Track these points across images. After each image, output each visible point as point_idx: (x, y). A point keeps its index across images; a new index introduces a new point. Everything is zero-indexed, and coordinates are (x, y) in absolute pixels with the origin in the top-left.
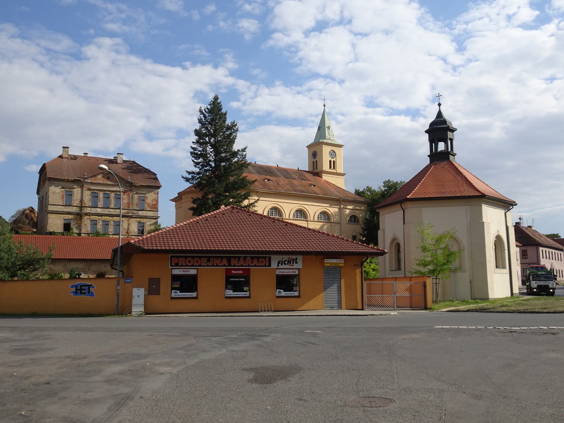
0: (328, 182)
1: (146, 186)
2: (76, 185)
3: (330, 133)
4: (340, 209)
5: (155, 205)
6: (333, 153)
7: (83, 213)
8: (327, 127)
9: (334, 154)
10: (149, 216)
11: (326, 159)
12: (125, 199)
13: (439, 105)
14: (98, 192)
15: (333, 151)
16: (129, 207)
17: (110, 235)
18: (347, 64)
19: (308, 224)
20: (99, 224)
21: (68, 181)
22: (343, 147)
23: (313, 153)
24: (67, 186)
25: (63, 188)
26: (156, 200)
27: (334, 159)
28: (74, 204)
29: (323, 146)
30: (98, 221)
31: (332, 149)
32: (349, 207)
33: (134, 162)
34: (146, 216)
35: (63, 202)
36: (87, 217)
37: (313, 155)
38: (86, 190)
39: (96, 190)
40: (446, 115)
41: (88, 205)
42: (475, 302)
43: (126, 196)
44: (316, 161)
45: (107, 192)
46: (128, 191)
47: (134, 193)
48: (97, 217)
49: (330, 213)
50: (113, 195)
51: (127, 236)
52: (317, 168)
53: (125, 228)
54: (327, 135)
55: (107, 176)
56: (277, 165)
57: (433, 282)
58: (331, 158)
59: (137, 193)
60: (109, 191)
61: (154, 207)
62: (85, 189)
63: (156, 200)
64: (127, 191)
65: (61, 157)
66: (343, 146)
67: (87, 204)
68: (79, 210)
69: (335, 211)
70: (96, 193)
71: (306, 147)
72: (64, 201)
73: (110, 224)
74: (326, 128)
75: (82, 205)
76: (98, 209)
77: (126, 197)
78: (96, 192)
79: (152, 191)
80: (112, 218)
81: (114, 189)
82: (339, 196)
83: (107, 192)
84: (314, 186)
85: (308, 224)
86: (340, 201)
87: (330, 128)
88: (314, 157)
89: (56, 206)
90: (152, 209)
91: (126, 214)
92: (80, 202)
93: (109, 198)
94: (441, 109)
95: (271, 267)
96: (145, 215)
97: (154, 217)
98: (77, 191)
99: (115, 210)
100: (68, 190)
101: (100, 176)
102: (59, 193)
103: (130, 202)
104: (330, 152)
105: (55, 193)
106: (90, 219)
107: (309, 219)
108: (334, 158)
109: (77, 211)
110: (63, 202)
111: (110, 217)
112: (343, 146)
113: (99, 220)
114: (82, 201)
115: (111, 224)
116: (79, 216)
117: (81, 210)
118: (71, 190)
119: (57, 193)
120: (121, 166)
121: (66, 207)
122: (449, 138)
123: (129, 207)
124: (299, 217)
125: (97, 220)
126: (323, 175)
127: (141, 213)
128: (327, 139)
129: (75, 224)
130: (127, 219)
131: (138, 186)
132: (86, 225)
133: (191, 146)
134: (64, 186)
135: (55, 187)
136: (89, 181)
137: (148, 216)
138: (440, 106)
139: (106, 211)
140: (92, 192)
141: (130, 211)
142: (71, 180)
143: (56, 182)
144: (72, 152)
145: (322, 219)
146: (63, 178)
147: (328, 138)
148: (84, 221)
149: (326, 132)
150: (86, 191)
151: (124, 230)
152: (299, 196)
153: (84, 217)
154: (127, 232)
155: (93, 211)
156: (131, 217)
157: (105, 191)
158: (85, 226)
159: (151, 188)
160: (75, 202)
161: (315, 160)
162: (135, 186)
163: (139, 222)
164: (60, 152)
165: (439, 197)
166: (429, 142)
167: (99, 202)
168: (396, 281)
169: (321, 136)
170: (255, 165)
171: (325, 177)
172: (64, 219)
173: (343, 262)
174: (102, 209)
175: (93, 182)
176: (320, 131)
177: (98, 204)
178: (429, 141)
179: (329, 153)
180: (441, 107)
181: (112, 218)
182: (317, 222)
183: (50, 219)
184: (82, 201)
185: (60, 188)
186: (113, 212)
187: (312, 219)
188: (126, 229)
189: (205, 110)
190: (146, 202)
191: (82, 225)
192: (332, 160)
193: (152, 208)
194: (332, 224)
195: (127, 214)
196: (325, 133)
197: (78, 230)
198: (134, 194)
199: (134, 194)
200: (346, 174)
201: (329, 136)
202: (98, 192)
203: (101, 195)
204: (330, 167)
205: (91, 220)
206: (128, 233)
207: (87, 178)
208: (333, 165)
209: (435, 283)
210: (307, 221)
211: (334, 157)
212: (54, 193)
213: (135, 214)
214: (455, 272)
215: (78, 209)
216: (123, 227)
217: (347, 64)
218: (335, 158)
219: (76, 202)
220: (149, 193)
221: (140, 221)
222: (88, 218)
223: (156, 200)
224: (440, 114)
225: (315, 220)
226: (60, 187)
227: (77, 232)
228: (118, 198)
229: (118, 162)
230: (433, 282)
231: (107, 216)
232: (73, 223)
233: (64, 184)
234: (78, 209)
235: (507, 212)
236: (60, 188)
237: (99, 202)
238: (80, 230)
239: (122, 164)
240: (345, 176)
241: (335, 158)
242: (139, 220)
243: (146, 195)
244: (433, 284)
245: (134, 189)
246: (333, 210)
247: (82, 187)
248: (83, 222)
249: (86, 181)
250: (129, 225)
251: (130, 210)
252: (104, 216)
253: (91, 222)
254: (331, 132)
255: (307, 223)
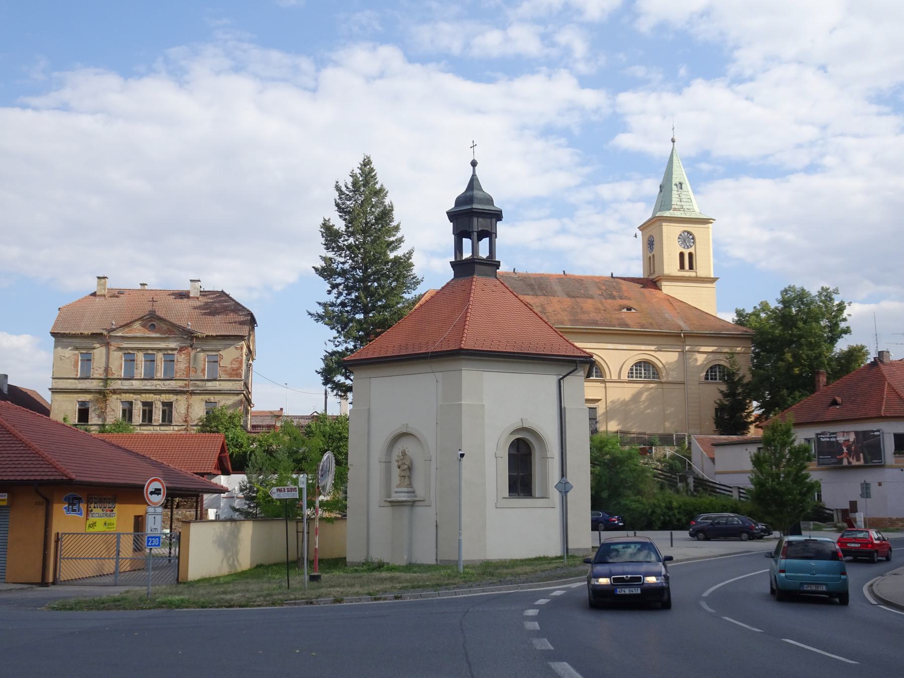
0: (671, 300)
1: (217, 336)
2: (98, 343)
3: (683, 196)
4: (683, 353)
5: (237, 370)
6: (687, 239)
7: (109, 389)
8: (676, 185)
9: (691, 237)
10: (224, 391)
11: (671, 250)
12: (181, 362)
14: (134, 352)
15: (688, 233)
16: (188, 375)
17: (155, 427)
18: (832, 30)
19: (605, 387)
20: (137, 408)
21: (82, 336)
22: (711, 223)
23: (649, 241)
24: (83, 345)
25: (76, 348)
26: (239, 360)
27: (692, 250)
28: (95, 376)
29: (663, 224)
30: (134, 403)
31: (686, 229)
32: (703, 349)
33: (222, 292)
34: (219, 390)
35: (75, 373)
36: (115, 396)
38: (115, 351)
39: (131, 349)
40: (487, 186)
41: (118, 376)
42: (513, 567)
43: (183, 356)
44: (653, 255)
45: (150, 352)
46: (186, 348)
47: (198, 350)
48: (132, 395)
49: (660, 365)
50: (160, 356)
51: (184, 427)
52: (654, 272)
53: (182, 412)
55: (150, 324)
56: (564, 272)
57: (297, 529)
58: (684, 248)
59: (203, 351)
60: (152, 349)
61: (235, 372)
62: (112, 348)
63: (238, 361)
64: (184, 347)
65: (94, 294)
66: (711, 221)
67: (116, 374)
68: (102, 386)
69: (669, 362)
70: (130, 353)
71: (638, 228)
72: (77, 371)
73: (156, 408)
74: (674, 187)
75: (107, 376)
76: (134, 382)
77: (183, 359)
78: (131, 352)
79: (232, 345)
80: (158, 397)
81: (163, 345)
82: (680, 327)
83: (150, 352)
84: (629, 309)
85: (605, 387)
86: (681, 336)
87: (683, 185)
88: (651, 249)
89: (64, 380)
90: (231, 377)
91: (183, 387)
92: (105, 370)
93: (154, 361)
94: (477, 173)
96: (218, 388)
97: (233, 390)
98: (99, 353)
99: (163, 382)
100: (85, 352)
101: (137, 325)
102: (70, 357)
103: (191, 366)
104: (681, 235)
105: (63, 358)
106: (120, 399)
107: (608, 377)
108: (691, 246)
109: (99, 386)
110: (75, 373)
111: (155, 395)
112: (711, 221)
113: (136, 400)
114: (107, 369)
115: (157, 406)
116: (103, 395)
117: (106, 385)
118: (90, 352)
119: (67, 358)
120: (197, 303)
121: (81, 381)
122: (475, 229)
123: (188, 375)
125: (133, 401)
126: (664, 283)
127: (210, 385)
129: (95, 410)
130: (185, 396)
131: (203, 338)
132: (113, 411)
134: (78, 345)
135: (63, 348)
136: (120, 334)
137: (222, 391)
138: (476, 166)
139: (149, 385)
140: (124, 352)
141: (192, 382)
142: (88, 334)
143: (65, 340)
144: (113, 283)
145: (641, 377)
146: (74, 332)
147: (677, 207)
148: (111, 404)
149: (673, 196)
150: (115, 352)
151: (180, 416)
152: (601, 333)
153: (111, 396)
154: (184, 419)
155: (127, 385)
156: (192, 393)
157: (147, 349)
158: (112, 413)
159: (226, 340)
160: (97, 372)
161: (651, 255)
162: (197, 338)
163: (206, 402)
164: (92, 285)
165: (375, 358)
167: (137, 369)
168: (138, 532)
169: (663, 203)
170: (514, 276)
171: (668, 289)
172: (78, 401)
173: (6, 498)
174: (141, 382)
175: (126, 335)
176: (662, 193)
177: (135, 372)
179: (679, 238)
180: (476, 167)
181: (159, 396)
182: (627, 382)
183: (55, 403)
184: (107, 369)
185: (71, 350)
186: (161, 385)
188: (184, 415)
190: (220, 366)
191: (107, 410)
193: (231, 375)
194: (665, 386)
195: (186, 388)
196: (671, 198)
197: (101, 420)
198: (198, 352)
199: (198, 352)
200: (718, 278)
201: (679, 203)
202: (134, 352)
203: (140, 356)
204: (682, 267)
205: (122, 401)
206: (186, 421)
207: (114, 330)
208: (687, 261)
209: (299, 533)
210: (604, 382)
211: (692, 244)
212: (61, 359)
213: (201, 387)
214: (412, 506)
215: (101, 384)
216: (178, 410)
217: (832, 30)
218: (694, 246)
219: (98, 372)
220: (224, 349)
221: (209, 399)
222: (117, 399)
223: (239, 360)
224: (473, 183)
226: (70, 348)
227: (100, 423)
228: (170, 361)
229: (191, 296)
230: (297, 529)
231: (150, 393)
232: (93, 408)
233: (77, 342)
234: (101, 384)
235: (562, 378)
236: (71, 350)
237: (137, 369)
238: (105, 419)
239: (198, 298)
240: (716, 282)
241: (694, 246)
242: (206, 397)
243: (220, 352)
244: (297, 532)
245: (198, 343)
246: (666, 358)
247: (108, 345)
248: (108, 406)
249: (113, 334)
250: (188, 407)
251: (191, 380)
252: (145, 393)
253: (122, 404)
254: (685, 193)
255: (603, 385)
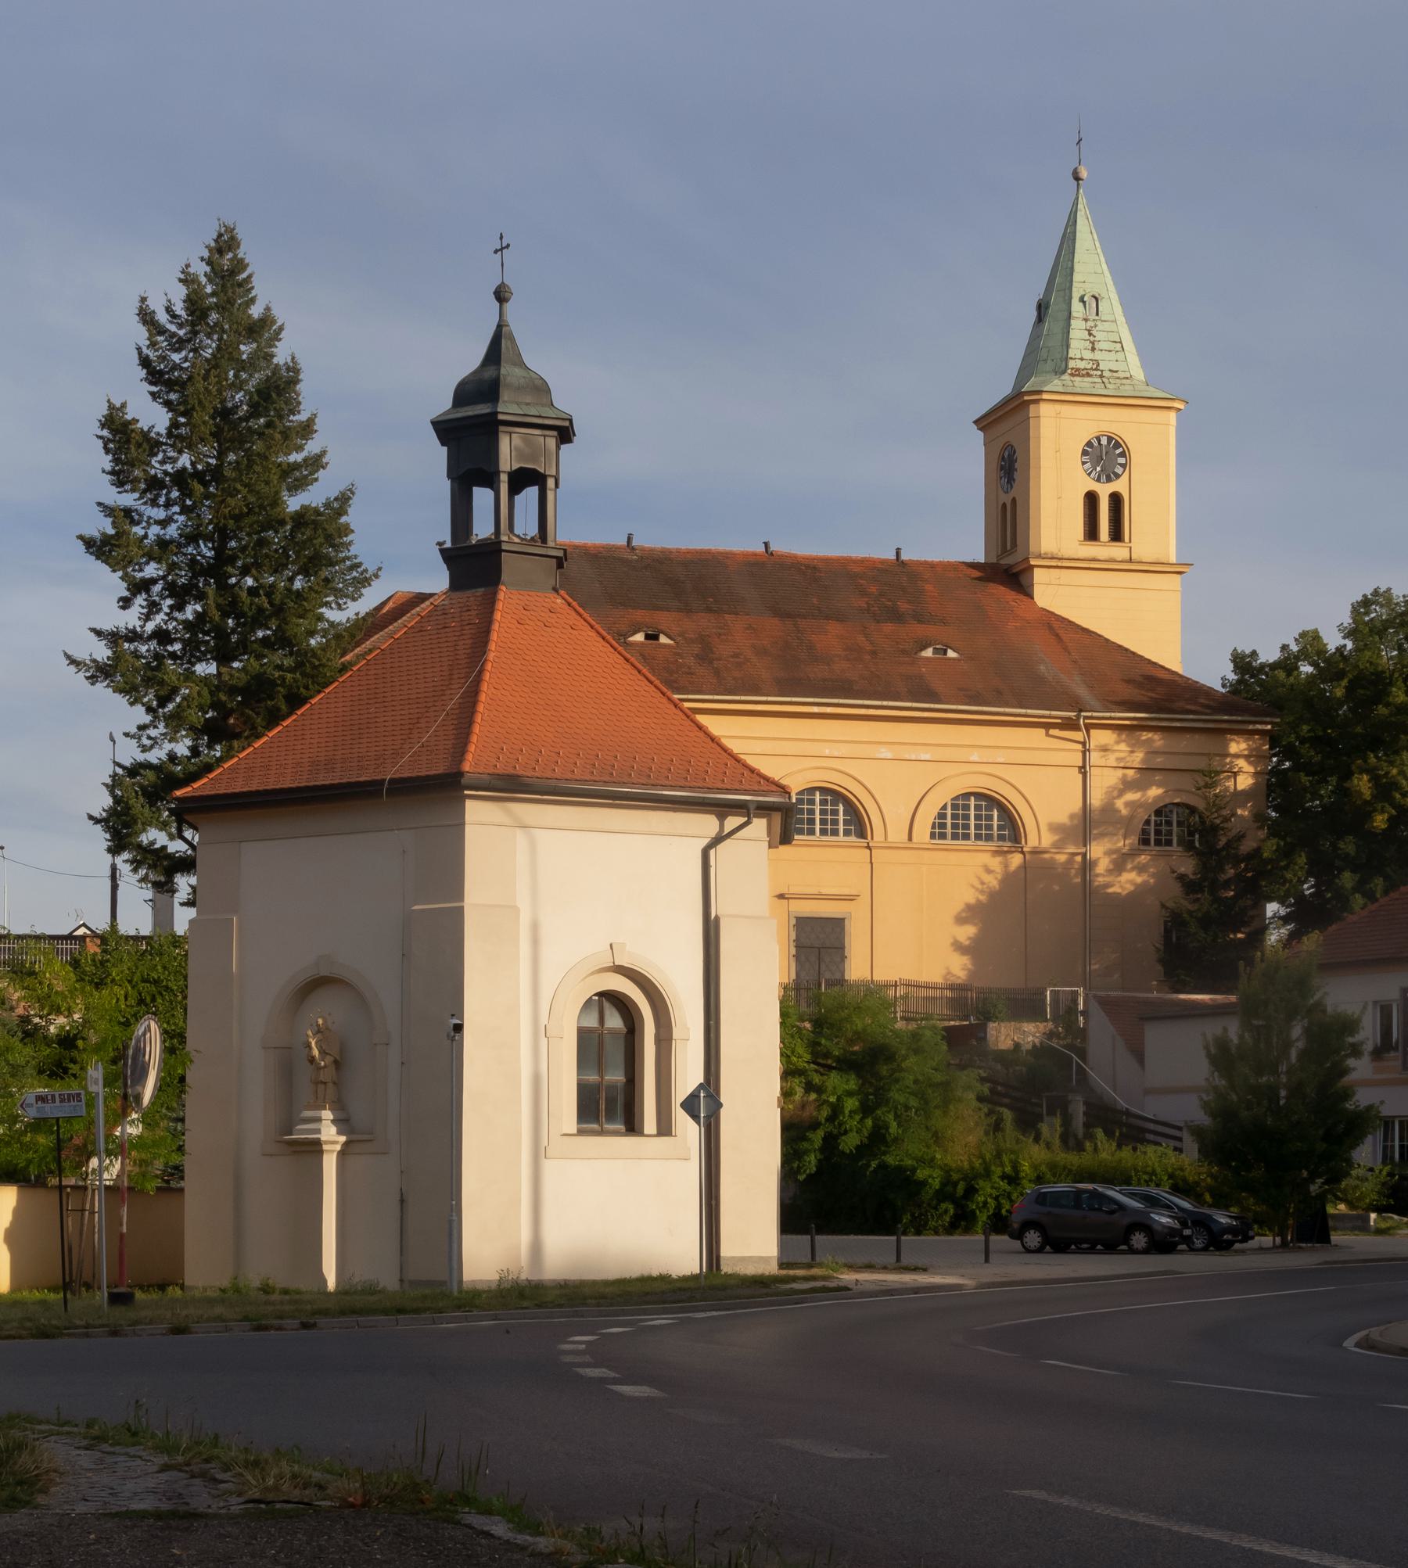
3: (1099, 336)
8: (1082, 300)
13: (501, 295)
37: (1002, 468)
44: (1014, 500)
54: (1078, 347)
74: (1077, 308)
95: (1047, 1115)
108: (1118, 476)
124: (818, 827)
128: (1077, 372)
133: (99, 504)
138: (506, 300)
147: (1082, 365)
161: (1104, 491)
166: (449, 482)
178: (449, 476)
187: (897, 834)
189: (169, 310)
192: (1104, 491)
201: (1088, 355)
204: (1092, 534)
225: (889, 840)
241: (1125, 476)
254: (1107, 326)
